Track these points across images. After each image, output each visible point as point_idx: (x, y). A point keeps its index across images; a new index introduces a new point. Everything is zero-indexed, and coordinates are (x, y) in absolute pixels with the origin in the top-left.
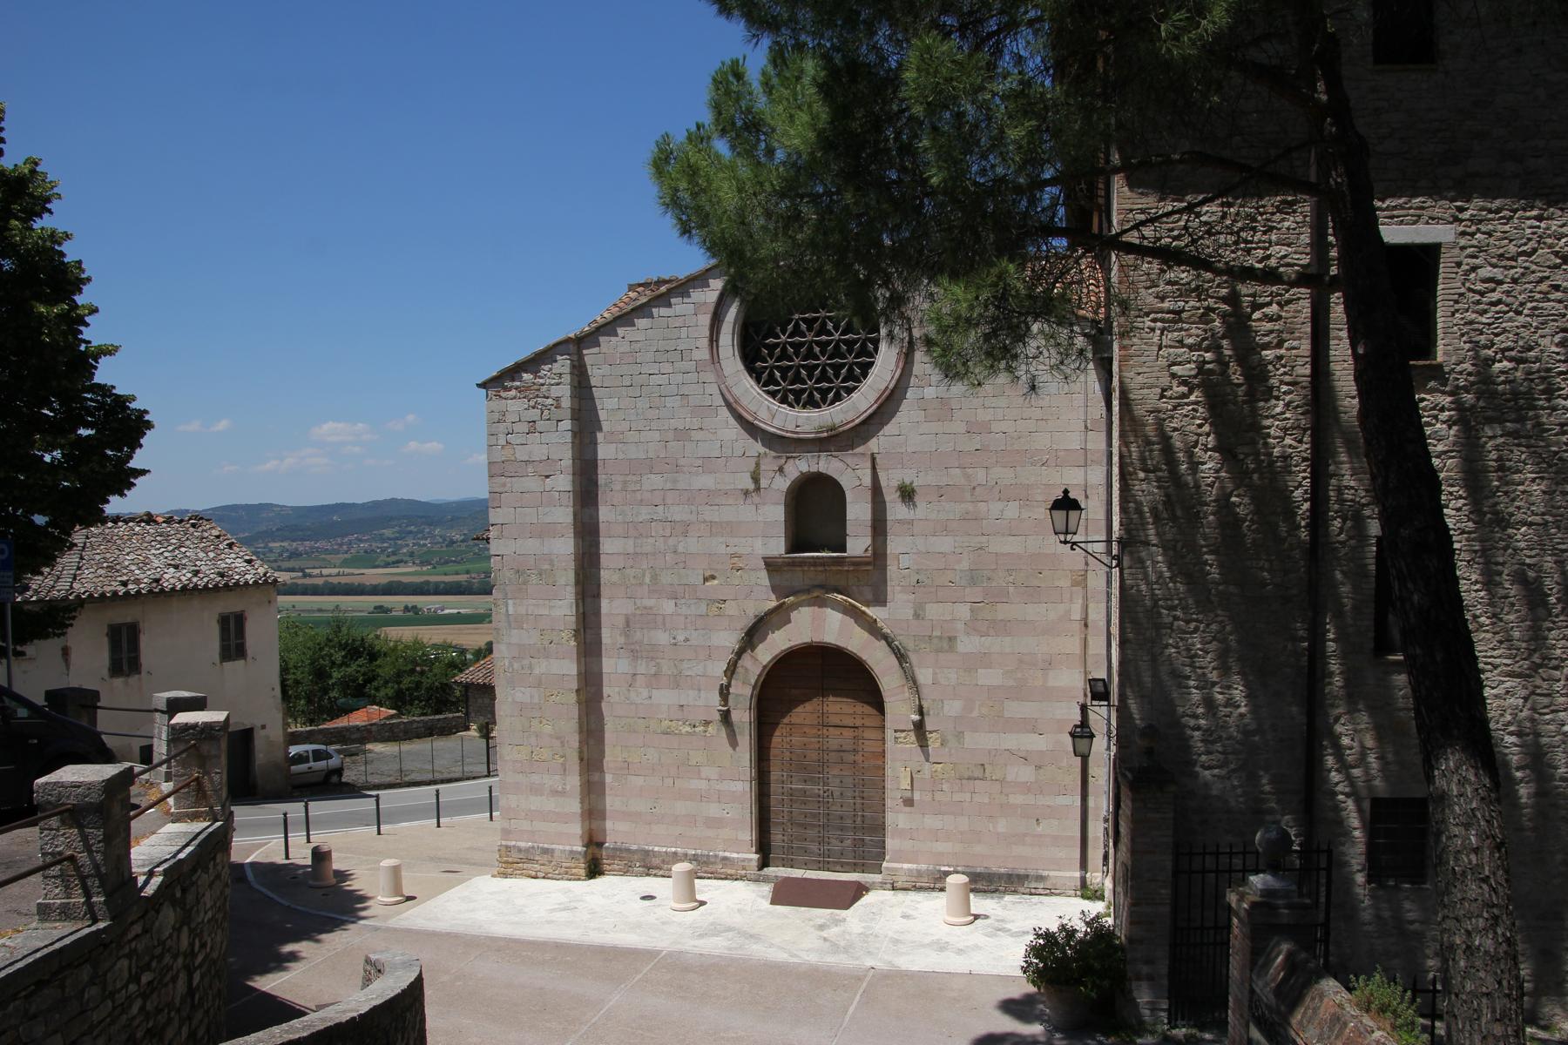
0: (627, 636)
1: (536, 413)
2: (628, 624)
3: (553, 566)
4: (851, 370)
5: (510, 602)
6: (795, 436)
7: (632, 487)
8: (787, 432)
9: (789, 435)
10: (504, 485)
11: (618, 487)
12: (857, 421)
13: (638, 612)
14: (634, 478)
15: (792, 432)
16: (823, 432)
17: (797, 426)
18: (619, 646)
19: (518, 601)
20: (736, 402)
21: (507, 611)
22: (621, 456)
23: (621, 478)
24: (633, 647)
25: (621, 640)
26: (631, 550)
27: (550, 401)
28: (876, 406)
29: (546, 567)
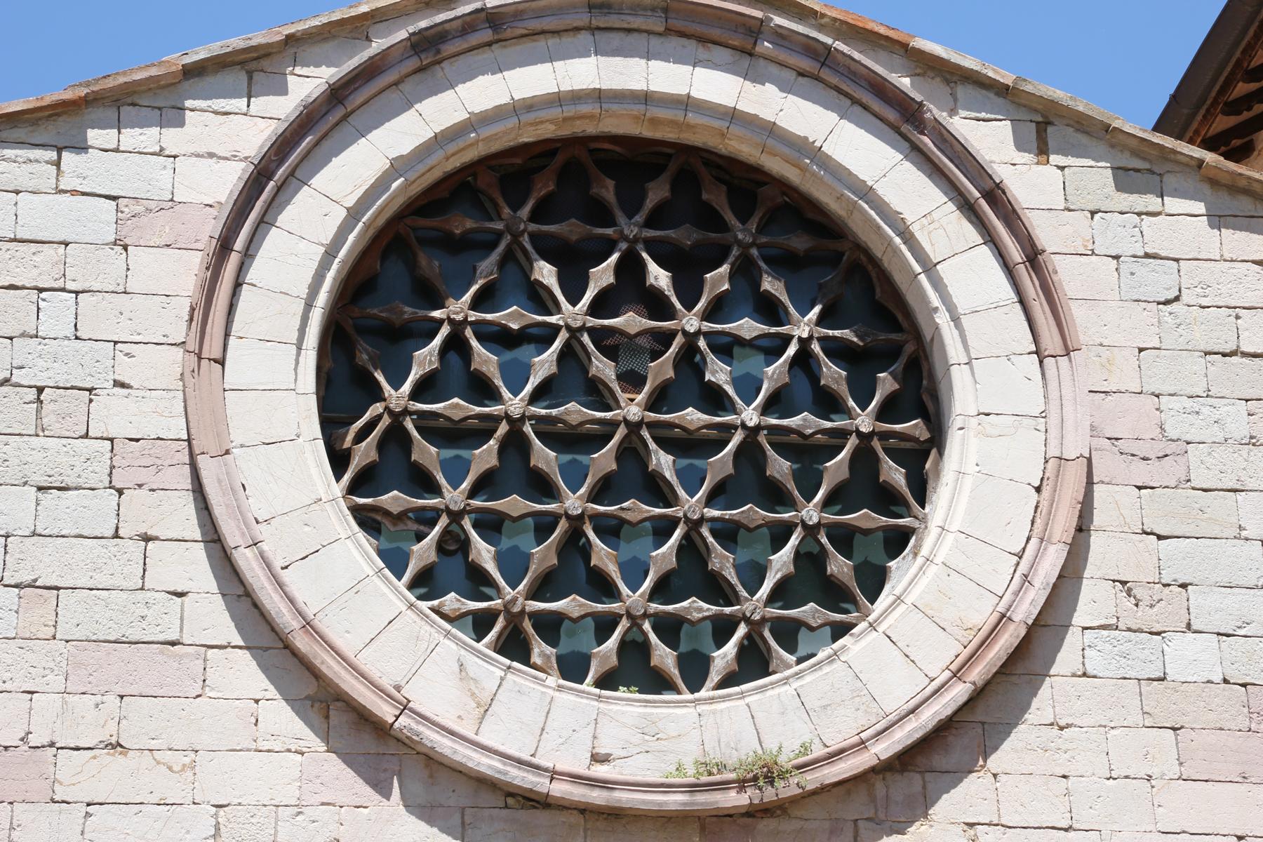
4: (810, 560)
6: (597, 797)
8: (554, 775)
9: (560, 789)
12: (884, 749)
15: (576, 778)
16: (722, 786)
17: (597, 758)
20: (308, 625)
28: (959, 693)
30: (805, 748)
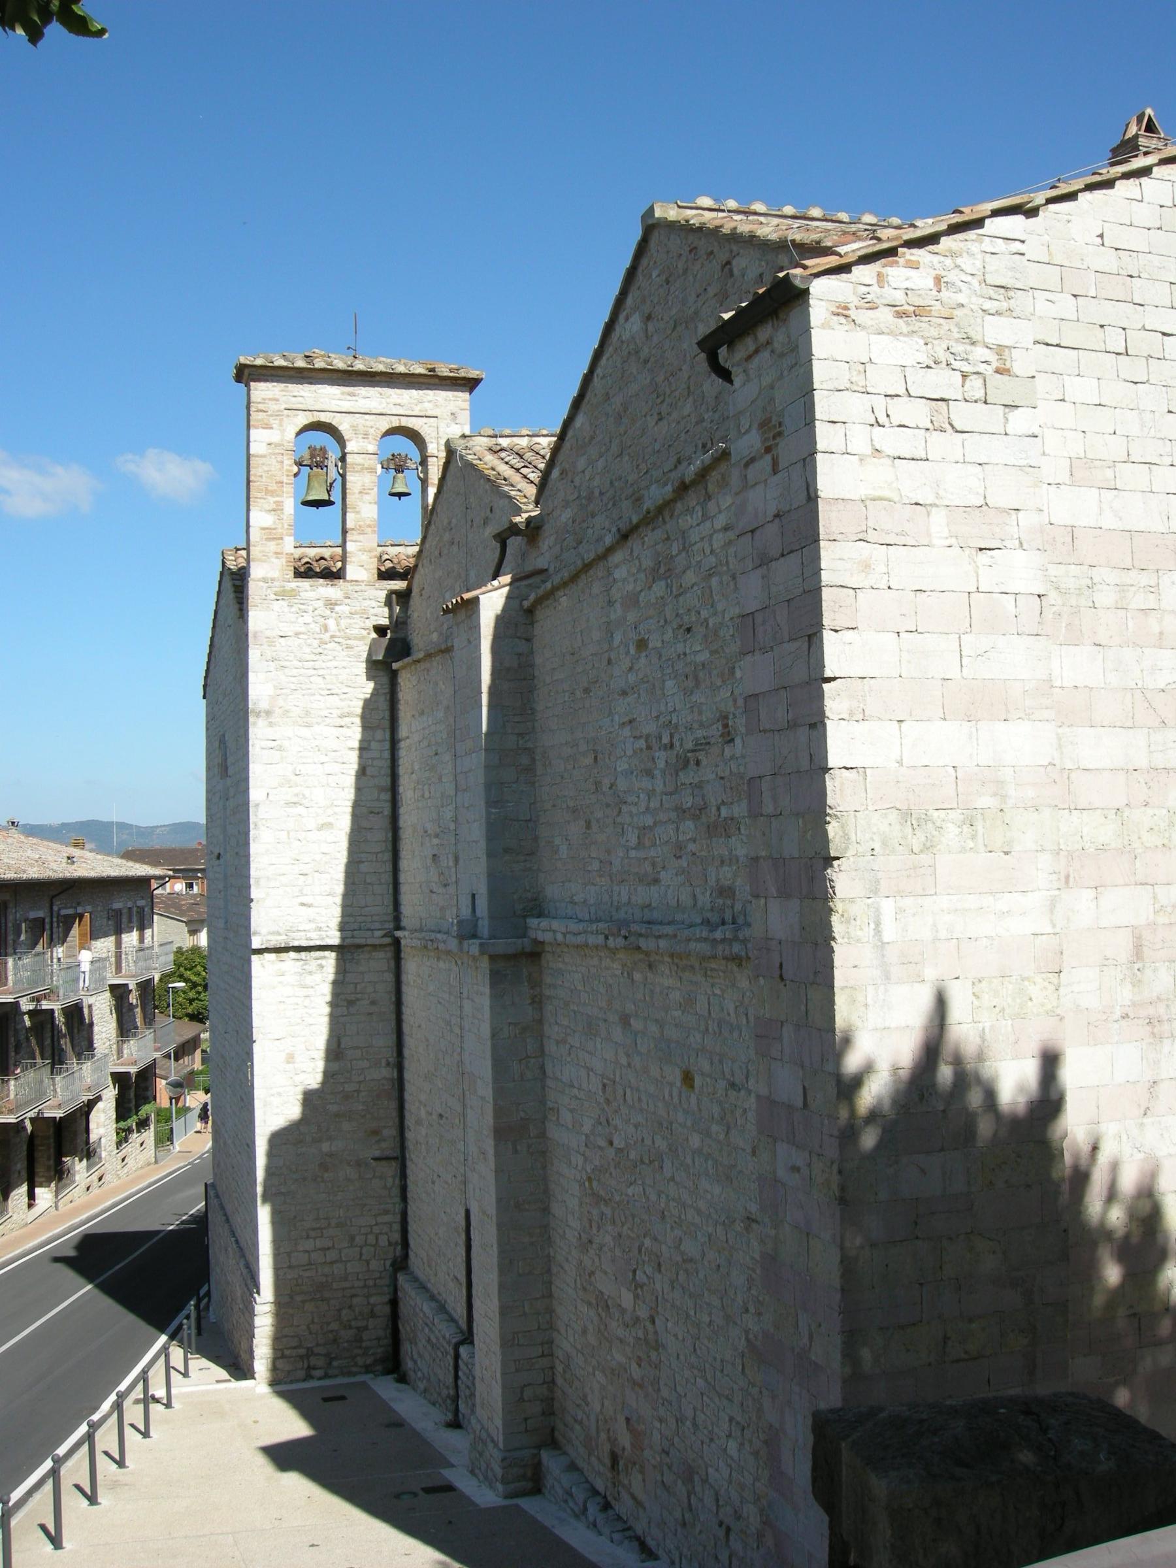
0: (1137, 983)
1: (944, 382)
2: (1138, 952)
3: (1004, 797)
5: (887, 907)
7: (1139, 600)
10: (866, 567)
11: (1105, 598)
13: (1162, 919)
14: (1145, 579)
18: (1118, 1013)
19: (908, 902)
21: (878, 931)
22: (1109, 522)
23: (1112, 577)
24: (1151, 1011)
25: (1126, 994)
26: (1142, 762)
27: (980, 353)
29: (985, 801)
30: (382, 789)
